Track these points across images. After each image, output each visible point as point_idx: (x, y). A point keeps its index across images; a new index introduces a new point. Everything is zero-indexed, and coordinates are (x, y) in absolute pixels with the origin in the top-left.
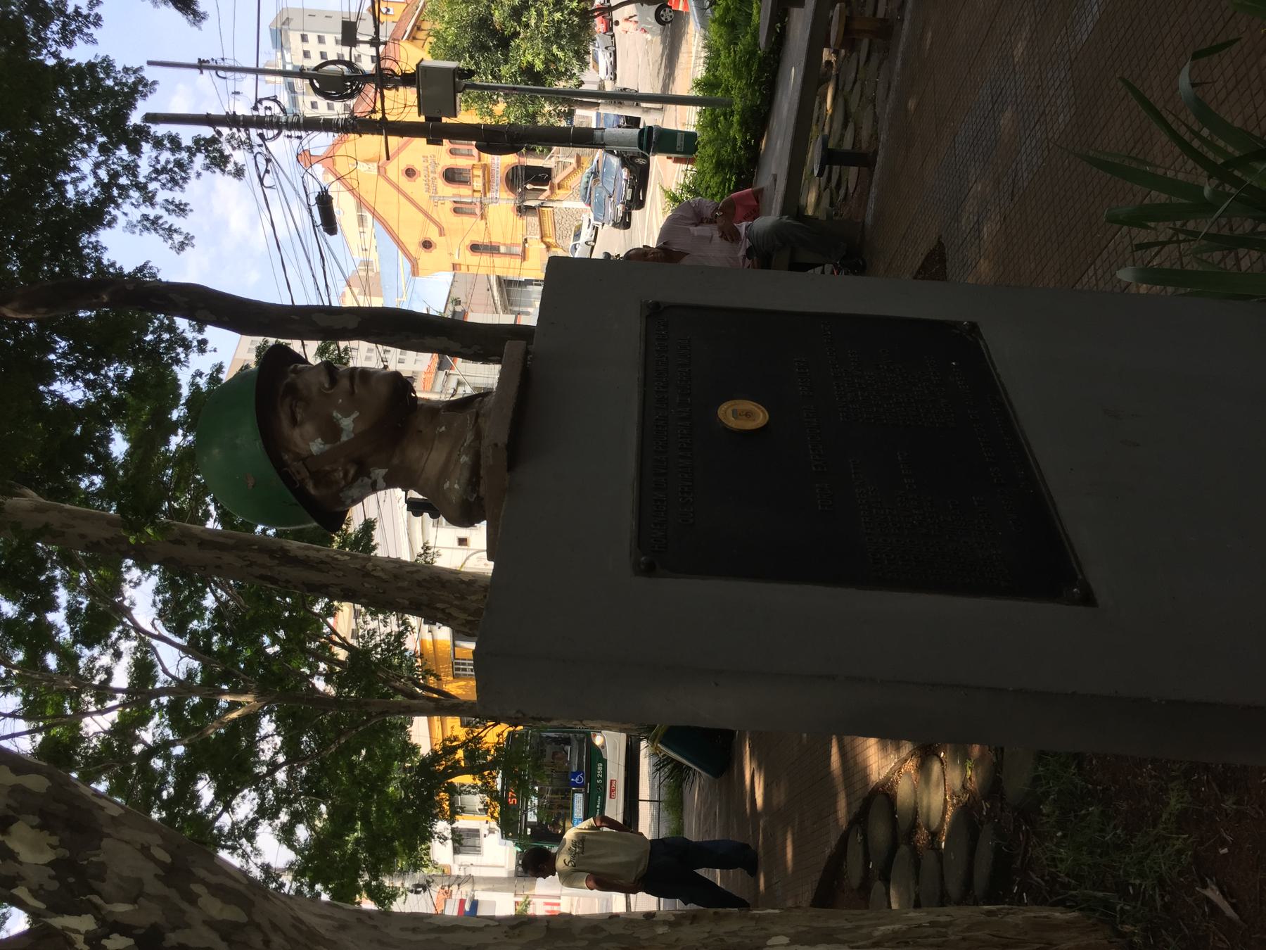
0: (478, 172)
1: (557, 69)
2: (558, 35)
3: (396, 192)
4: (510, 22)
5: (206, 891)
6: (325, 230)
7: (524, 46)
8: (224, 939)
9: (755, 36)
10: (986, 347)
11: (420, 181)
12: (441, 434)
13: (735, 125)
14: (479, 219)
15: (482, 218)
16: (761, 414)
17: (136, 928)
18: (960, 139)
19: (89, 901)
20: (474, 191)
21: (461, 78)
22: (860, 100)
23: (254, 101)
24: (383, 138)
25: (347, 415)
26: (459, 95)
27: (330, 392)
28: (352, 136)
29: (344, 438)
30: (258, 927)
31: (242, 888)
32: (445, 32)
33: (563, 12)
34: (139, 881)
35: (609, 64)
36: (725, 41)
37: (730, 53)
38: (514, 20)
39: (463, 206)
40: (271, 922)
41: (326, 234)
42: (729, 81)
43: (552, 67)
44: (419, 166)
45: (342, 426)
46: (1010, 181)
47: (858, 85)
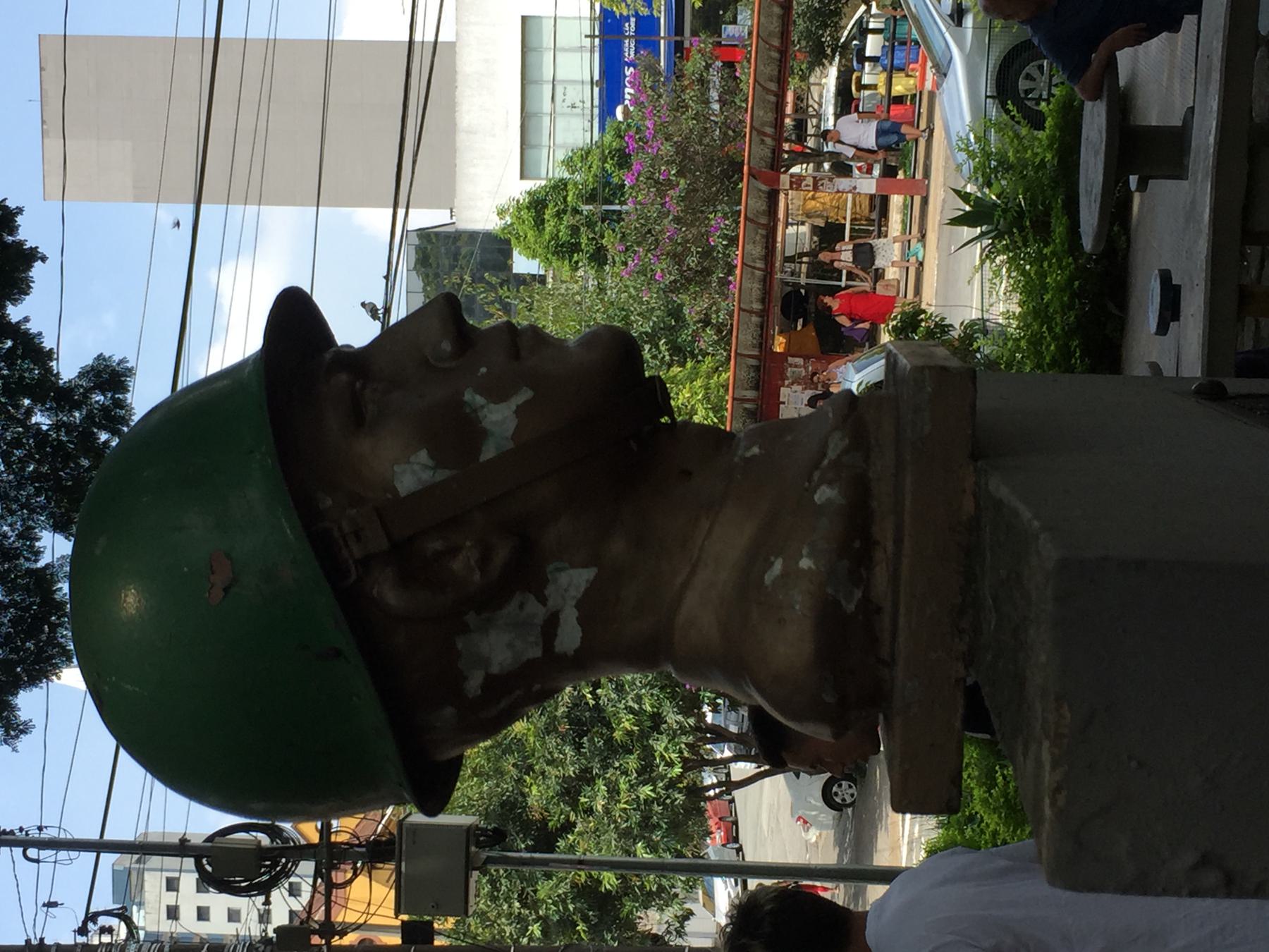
1: (642, 887)
2: (647, 824)
23: (82, 917)
26: (476, 874)
29: (489, 452)
33: (654, 785)
38: (566, 803)
45: (486, 424)
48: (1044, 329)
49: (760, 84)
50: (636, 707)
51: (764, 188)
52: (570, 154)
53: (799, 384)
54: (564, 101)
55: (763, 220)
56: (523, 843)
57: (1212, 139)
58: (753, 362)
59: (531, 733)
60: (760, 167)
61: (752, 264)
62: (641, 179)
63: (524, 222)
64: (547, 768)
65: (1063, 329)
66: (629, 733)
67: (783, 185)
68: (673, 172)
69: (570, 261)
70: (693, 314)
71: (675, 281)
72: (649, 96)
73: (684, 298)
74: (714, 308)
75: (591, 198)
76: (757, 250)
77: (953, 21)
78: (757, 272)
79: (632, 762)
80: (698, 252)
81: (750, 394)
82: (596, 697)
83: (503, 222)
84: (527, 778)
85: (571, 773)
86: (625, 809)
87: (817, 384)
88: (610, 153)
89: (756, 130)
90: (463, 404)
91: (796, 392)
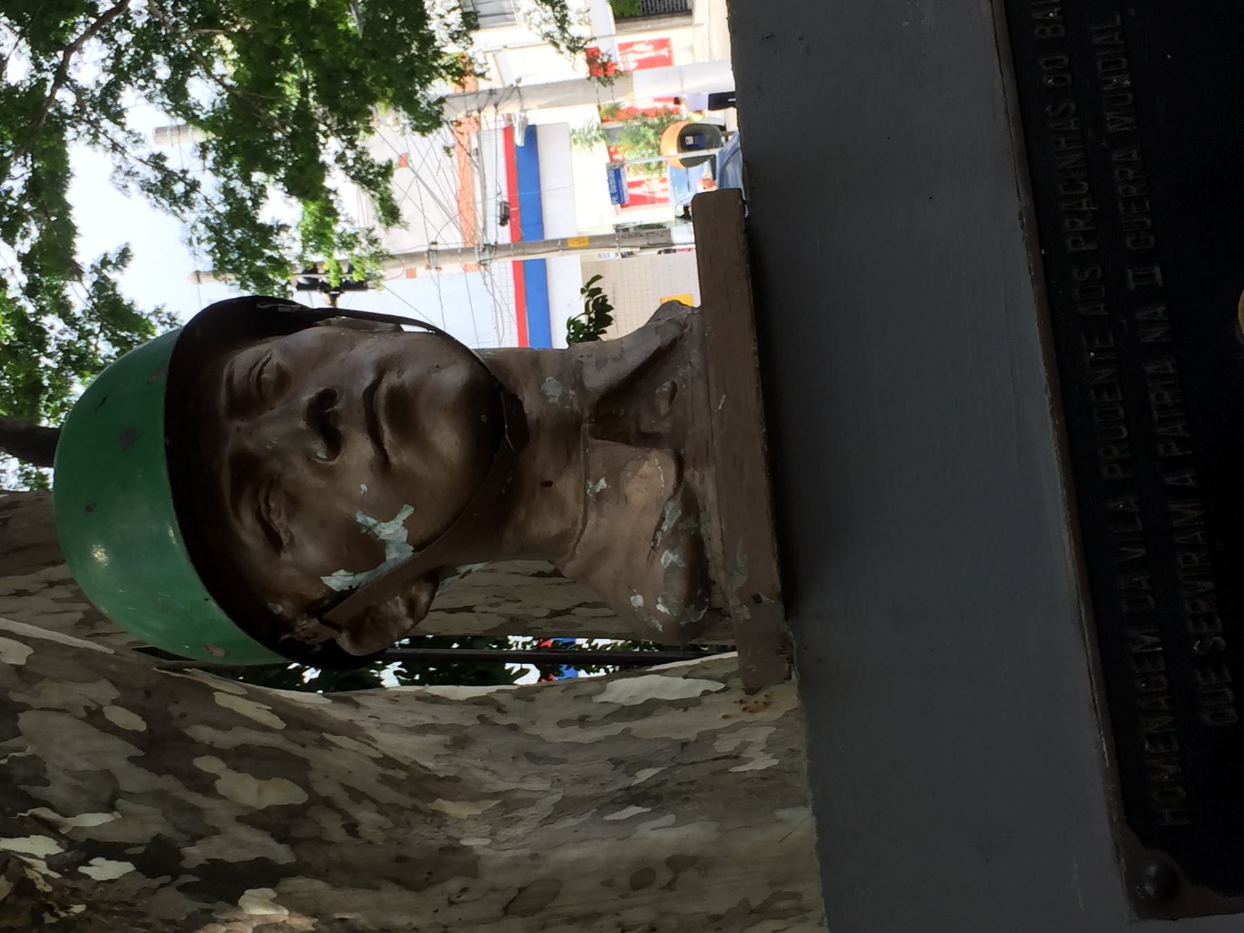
5: (224, 765)
8: (280, 841)
12: (599, 496)
17: (129, 846)
19: (34, 817)
25: (390, 517)
30: (328, 803)
31: (276, 741)
34: (107, 774)
40: (348, 789)
45: (382, 537)
87: (105, 362)
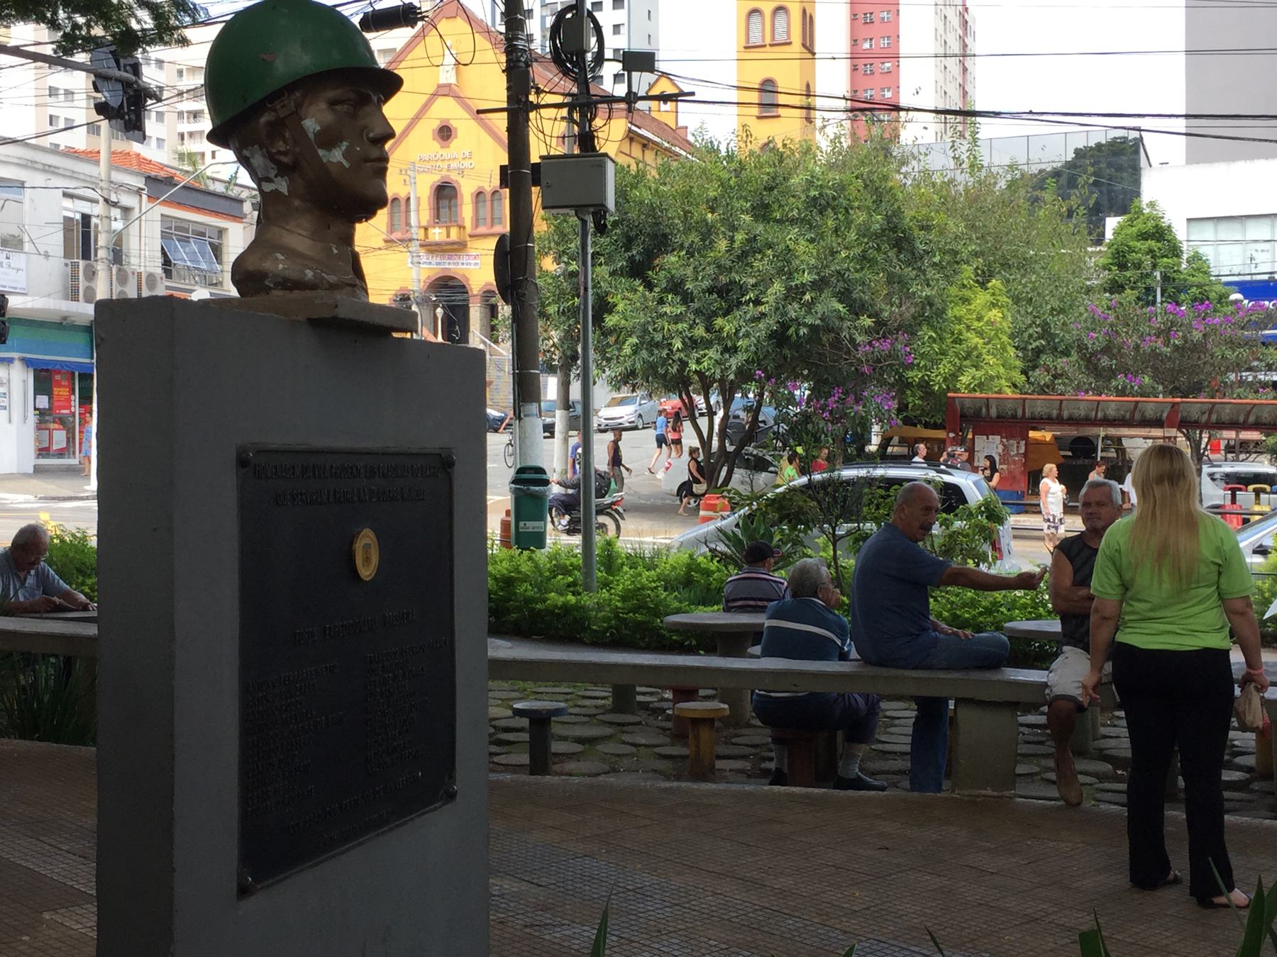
0: (454, 234)
1: (608, 345)
3: (411, 114)
4: (665, 278)
6: (366, 15)
7: (635, 297)
9: (678, 611)
10: (435, 809)
11: (434, 147)
13: (562, 599)
14: (385, 237)
15: (386, 241)
16: (368, 573)
18: (587, 862)
20: (426, 229)
21: (594, 214)
22: (612, 754)
24: (505, 105)
27: (365, 138)
28: (503, 58)
29: (321, 152)
32: (645, 186)
35: (619, 421)
36: (668, 575)
37: (654, 581)
39: (403, 215)
41: (361, 16)
42: (618, 585)
43: (611, 340)
44: (457, 145)
45: (334, 151)
46: (548, 921)
47: (633, 749)
48: (981, 609)
49: (1252, 408)
50: (741, 334)
51: (1165, 415)
52: (1204, 258)
53: (1004, 450)
54: (1256, 250)
55: (1137, 416)
56: (637, 253)
57: (1022, 678)
58: (1020, 413)
59: (717, 253)
60: (1181, 411)
61: (1100, 409)
62: (1171, 316)
63: (1145, 223)
64: (691, 268)
65: (981, 622)
66: (721, 330)
67: (1168, 431)
68: (1176, 342)
69: (1111, 264)
70: (1061, 365)
71: (1087, 348)
72: (1243, 319)
73: (1075, 356)
74: (1066, 381)
75: (1166, 278)
76: (1111, 412)
77: (1258, 547)
78: (1094, 413)
79: (700, 331)
80: (1111, 365)
81: (993, 412)
82: (747, 303)
83: (1145, 207)
84: (684, 253)
85: (687, 286)
86: (664, 329)
88: (1205, 291)
89: (1213, 407)
90: (341, 142)
91: (997, 448)
